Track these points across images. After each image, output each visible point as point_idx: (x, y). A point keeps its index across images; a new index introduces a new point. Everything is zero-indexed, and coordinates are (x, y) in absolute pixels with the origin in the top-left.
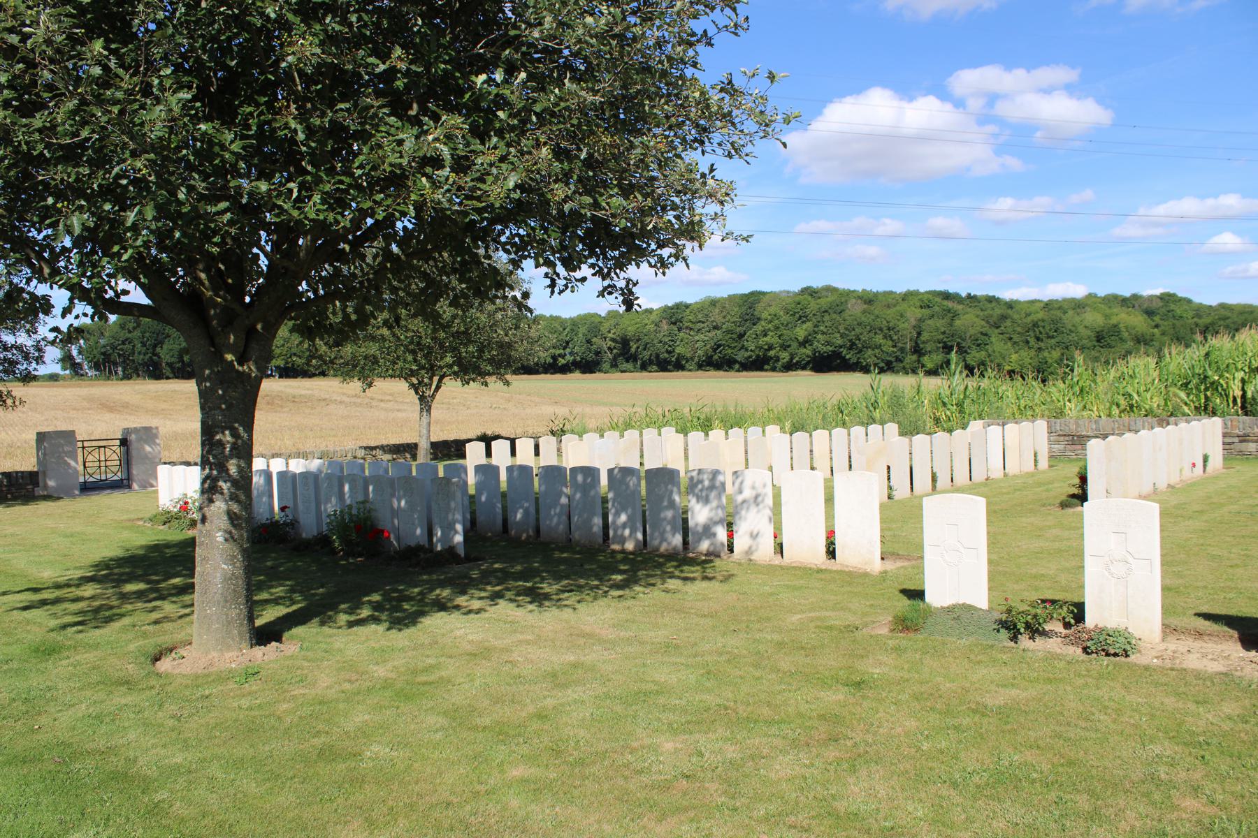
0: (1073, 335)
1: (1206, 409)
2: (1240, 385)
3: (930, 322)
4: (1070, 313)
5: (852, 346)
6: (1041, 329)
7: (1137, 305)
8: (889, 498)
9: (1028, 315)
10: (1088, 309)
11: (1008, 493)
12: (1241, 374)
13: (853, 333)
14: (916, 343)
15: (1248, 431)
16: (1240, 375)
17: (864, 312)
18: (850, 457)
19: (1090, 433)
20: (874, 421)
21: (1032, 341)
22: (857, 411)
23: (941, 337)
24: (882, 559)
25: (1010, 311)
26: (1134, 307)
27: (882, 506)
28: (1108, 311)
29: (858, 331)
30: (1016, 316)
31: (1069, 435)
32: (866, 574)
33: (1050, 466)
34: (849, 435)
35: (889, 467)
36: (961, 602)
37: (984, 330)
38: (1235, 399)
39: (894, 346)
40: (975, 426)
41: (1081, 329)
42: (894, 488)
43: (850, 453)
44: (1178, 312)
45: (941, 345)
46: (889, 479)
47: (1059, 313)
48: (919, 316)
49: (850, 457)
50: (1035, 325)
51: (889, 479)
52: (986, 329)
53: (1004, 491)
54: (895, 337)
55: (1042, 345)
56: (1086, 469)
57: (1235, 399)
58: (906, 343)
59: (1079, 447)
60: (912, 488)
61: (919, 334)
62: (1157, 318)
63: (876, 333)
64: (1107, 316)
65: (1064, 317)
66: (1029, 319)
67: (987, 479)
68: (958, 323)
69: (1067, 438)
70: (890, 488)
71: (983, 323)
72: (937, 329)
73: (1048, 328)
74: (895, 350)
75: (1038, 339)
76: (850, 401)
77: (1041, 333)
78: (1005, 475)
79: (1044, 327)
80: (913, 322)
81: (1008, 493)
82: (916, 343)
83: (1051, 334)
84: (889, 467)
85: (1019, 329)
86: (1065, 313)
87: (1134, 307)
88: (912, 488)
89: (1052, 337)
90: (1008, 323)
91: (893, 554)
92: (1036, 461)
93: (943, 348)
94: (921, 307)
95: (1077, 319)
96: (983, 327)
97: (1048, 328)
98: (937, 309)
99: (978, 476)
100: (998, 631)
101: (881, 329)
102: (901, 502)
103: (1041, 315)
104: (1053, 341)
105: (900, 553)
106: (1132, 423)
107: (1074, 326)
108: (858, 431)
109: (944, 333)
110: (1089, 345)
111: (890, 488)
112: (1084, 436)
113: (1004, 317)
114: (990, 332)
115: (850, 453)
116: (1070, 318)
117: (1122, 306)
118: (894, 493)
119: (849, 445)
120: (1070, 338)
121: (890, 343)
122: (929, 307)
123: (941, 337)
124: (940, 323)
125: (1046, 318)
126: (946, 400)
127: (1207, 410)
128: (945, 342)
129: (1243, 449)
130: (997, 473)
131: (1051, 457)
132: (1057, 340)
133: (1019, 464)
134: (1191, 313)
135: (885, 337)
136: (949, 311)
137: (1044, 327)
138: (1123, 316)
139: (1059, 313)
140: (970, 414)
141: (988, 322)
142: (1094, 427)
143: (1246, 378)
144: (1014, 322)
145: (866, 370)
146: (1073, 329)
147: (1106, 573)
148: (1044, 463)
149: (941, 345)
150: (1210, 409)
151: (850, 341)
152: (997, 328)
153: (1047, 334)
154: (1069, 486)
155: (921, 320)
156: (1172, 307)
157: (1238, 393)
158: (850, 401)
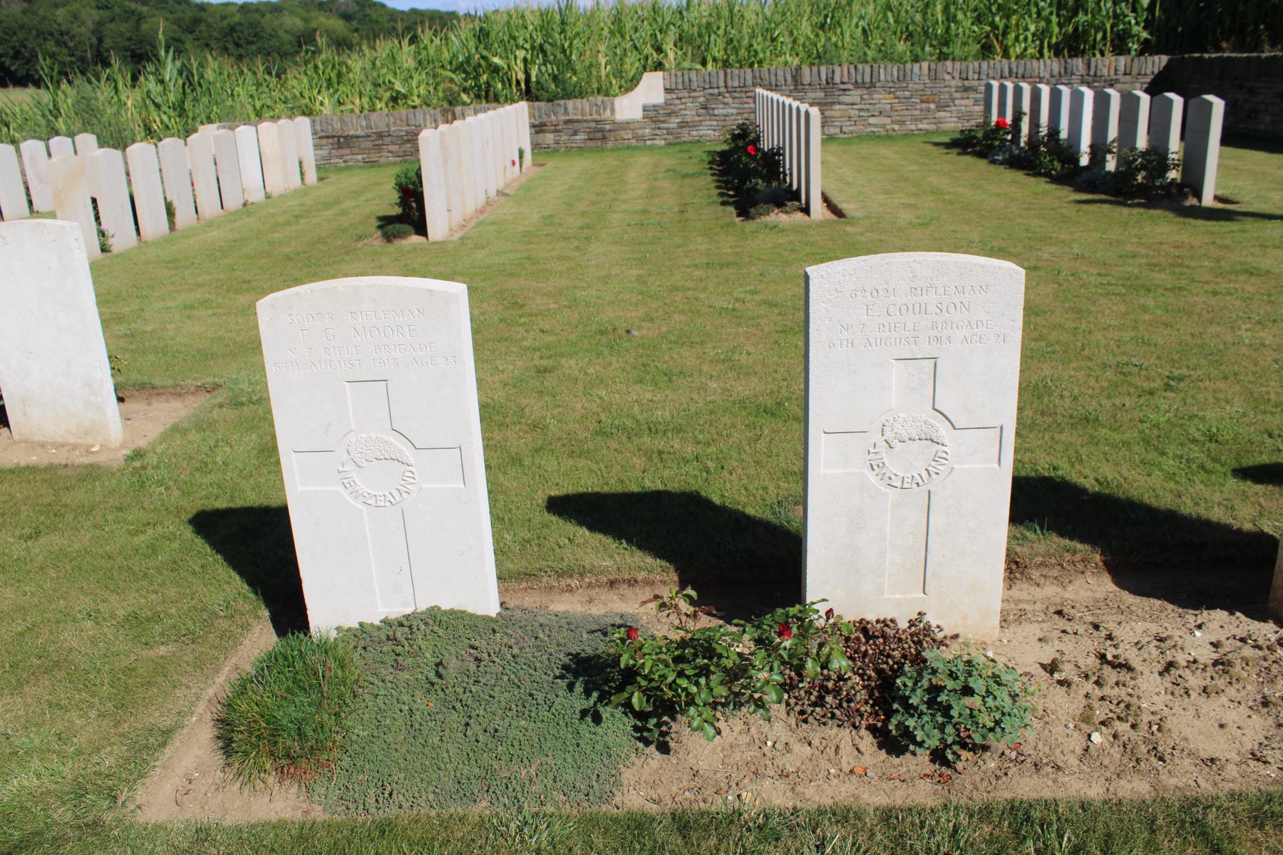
0: (274, 40)
1: (487, 97)
2: (522, 66)
3: (112, 26)
4: (269, 16)
5: (17, 55)
6: (240, 35)
7: (334, 9)
8: (104, 249)
9: (224, 18)
10: (285, 12)
11: (288, 223)
12: (521, 54)
13: (15, 38)
14: (98, 51)
15: (545, 119)
16: (521, 54)
17: (24, 12)
18: (27, 189)
19: (360, 133)
20: (57, 133)
21: (231, 47)
22: (31, 123)
23: (127, 43)
24: (120, 400)
25: (202, 14)
26: (331, 11)
27: (94, 267)
28: (305, 14)
29: (21, 35)
30: (210, 20)
31: (333, 137)
32: (92, 473)
33: (320, 179)
34: (20, 156)
35: (94, 201)
36: (423, 607)
37: (176, 35)
38: (518, 83)
39: (73, 55)
40: (208, 134)
41: (281, 33)
42: (109, 232)
43: (25, 183)
44: (374, 16)
45: (129, 53)
46: (97, 218)
47: (257, 16)
48: (97, 18)
49: (27, 189)
50: (232, 29)
51: (97, 218)
52: (179, 34)
53: (281, 219)
54: (71, 44)
55: (242, 51)
56: (419, 176)
57: (518, 83)
58: (86, 51)
59: (348, 151)
60: (138, 230)
61: (100, 40)
62: (355, 23)
63: (45, 39)
64: (306, 20)
65: (263, 21)
66: (225, 23)
67: (245, 205)
68: (144, 27)
69: (331, 141)
70: (102, 234)
71: (174, 27)
72: (122, 35)
73: (246, 33)
74: (73, 59)
75: (238, 45)
76: (17, 110)
77: (240, 38)
78: (268, 197)
79: (242, 32)
80: (92, 27)
81: (288, 223)
82: (98, 51)
83: (251, 39)
84: (94, 201)
85: (215, 34)
86: (263, 16)
87: (331, 11)
88: (138, 230)
89: (253, 43)
90: (203, 27)
91: (142, 387)
92: (302, 174)
93: (132, 57)
94: (98, 8)
95: (276, 23)
96: (174, 32)
97: (246, 33)
98: (117, 10)
99: (233, 202)
100: (597, 719)
101: (51, 34)
102: (125, 256)
103: (237, 18)
104: (254, 48)
105: (157, 381)
106: (411, 116)
107: (274, 30)
108: (32, 147)
109: (130, 39)
110: (292, 50)
111: (102, 234)
112: (352, 137)
113: (197, 21)
114: (184, 37)
115: (25, 183)
116: (268, 21)
117: (319, 10)
118: (110, 241)
119: (24, 174)
120: (271, 43)
121: (66, 51)
122: (107, 8)
123: (127, 43)
124: (124, 27)
125: (243, 21)
126: (159, 100)
127: (487, 96)
128: (132, 50)
129: (540, 141)
130: (257, 196)
131: (318, 168)
132: (258, 45)
133: (283, 180)
134: (386, 18)
135: (58, 43)
136: (133, 13)
137: (242, 32)
138: (322, 19)
139: (257, 16)
140: (194, 119)
141: (179, 26)
142: (364, 124)
143: (529, 57)
144: (209, 26)
145: (38, 83)
146: (273, 33)
147: (873, 479)
148: (312, 176)
149: (129, 53)
150: (491, 95)
151: (13, 48)
152: (191, 32)
153: (246, 39)
154: (388, 202)
155: (100, 24)
156: (368, 11)
157: (521, 76)
158: (17, 110)
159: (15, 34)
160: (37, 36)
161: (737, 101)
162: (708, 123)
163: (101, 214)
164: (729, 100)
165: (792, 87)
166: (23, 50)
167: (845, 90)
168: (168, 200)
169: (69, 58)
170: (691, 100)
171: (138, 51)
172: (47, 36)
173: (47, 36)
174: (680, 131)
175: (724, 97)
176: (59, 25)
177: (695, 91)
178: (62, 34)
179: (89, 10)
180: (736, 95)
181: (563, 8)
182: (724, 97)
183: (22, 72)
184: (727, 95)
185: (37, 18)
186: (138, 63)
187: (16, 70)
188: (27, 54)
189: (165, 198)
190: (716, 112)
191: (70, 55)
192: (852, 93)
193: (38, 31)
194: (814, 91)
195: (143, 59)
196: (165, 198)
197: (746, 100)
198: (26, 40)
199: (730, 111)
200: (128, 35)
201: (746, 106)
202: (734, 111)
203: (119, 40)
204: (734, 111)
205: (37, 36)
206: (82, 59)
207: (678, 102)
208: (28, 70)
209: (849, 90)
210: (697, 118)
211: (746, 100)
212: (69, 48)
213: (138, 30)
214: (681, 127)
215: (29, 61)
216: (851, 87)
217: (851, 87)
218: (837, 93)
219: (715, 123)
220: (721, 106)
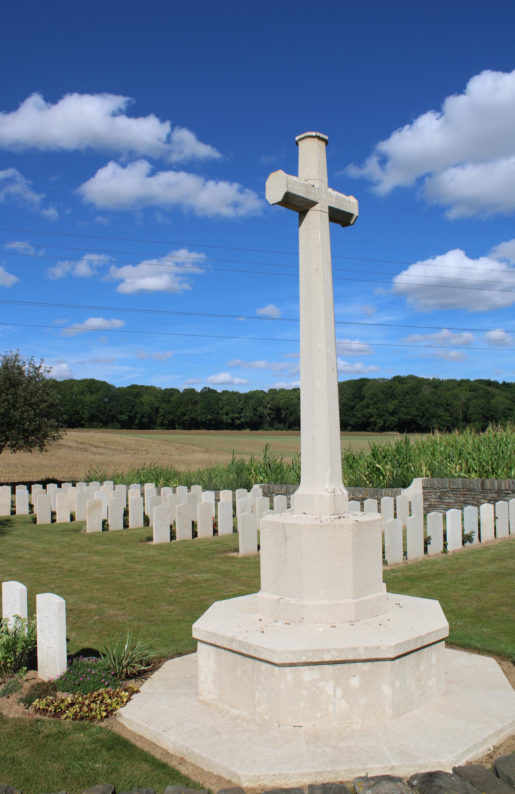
3: (474, 401)
23: (481, 411)
29: (427, 405)
37: (509, 406)
39: (451, 416)
63: (439, 408)
74: (452, 419)
94: (470, 391)
109: (483, 408)
121: (448, 414)
122: (475, 390)
123: (481, 411)
124: (482, 402)
128: (483, 415)
151: (422, 412)
155: (469, 400)
159: (424, 405)
160: (435, 407)
161: (455, 496)
162: (441, 506)
163: (494, 530)
164: (452, 495)
165: (481, 490)
166: (427, 413)
167: (507, 494)
168: (146, 514)
169: (449, 418)
170: (434, 493)
171: (486, 415)
172: (440, 406)
173: (440, 406)
174: (429, 509)
175: (449, 493)
176: (447, 400)
177: (435, 489)
178: (448, 405)
179: (464, 392)
180: (454, 493)
181: (399, 442)
182: (449, 493)
183: (425, 425)
184: (450, 492)
185: (437, 397)
186: (486, 422)
187: (422, 424)
188: (428, 416)
189: (144, 513)
190: (445, 501)
191: (450, 417)
192: (511, 495)
193: (436, 404)
194: (492, 493)
195: (489, 420)
196: (144, 513)
197: (459, 495)
198: (429, 408)
199: (451, 500)
200: (483, 405)
201: (459, 499)
202: (453, 501)
203: (477, 408)
204: (453, 501)
205: (435, 407)
206: (456, 419)
207: (428, 494)
208: (428, 424)
209: (509, 494)
210: (436, 503)
211: (459, 495)
212: (450, 413)
213: (489, 403)
214: (430, 507)
215: (428, 419)
216: (510, 492)
217: (510, 492)
218: (503, 495)
219: (445, 506)
220: (447, 498)
